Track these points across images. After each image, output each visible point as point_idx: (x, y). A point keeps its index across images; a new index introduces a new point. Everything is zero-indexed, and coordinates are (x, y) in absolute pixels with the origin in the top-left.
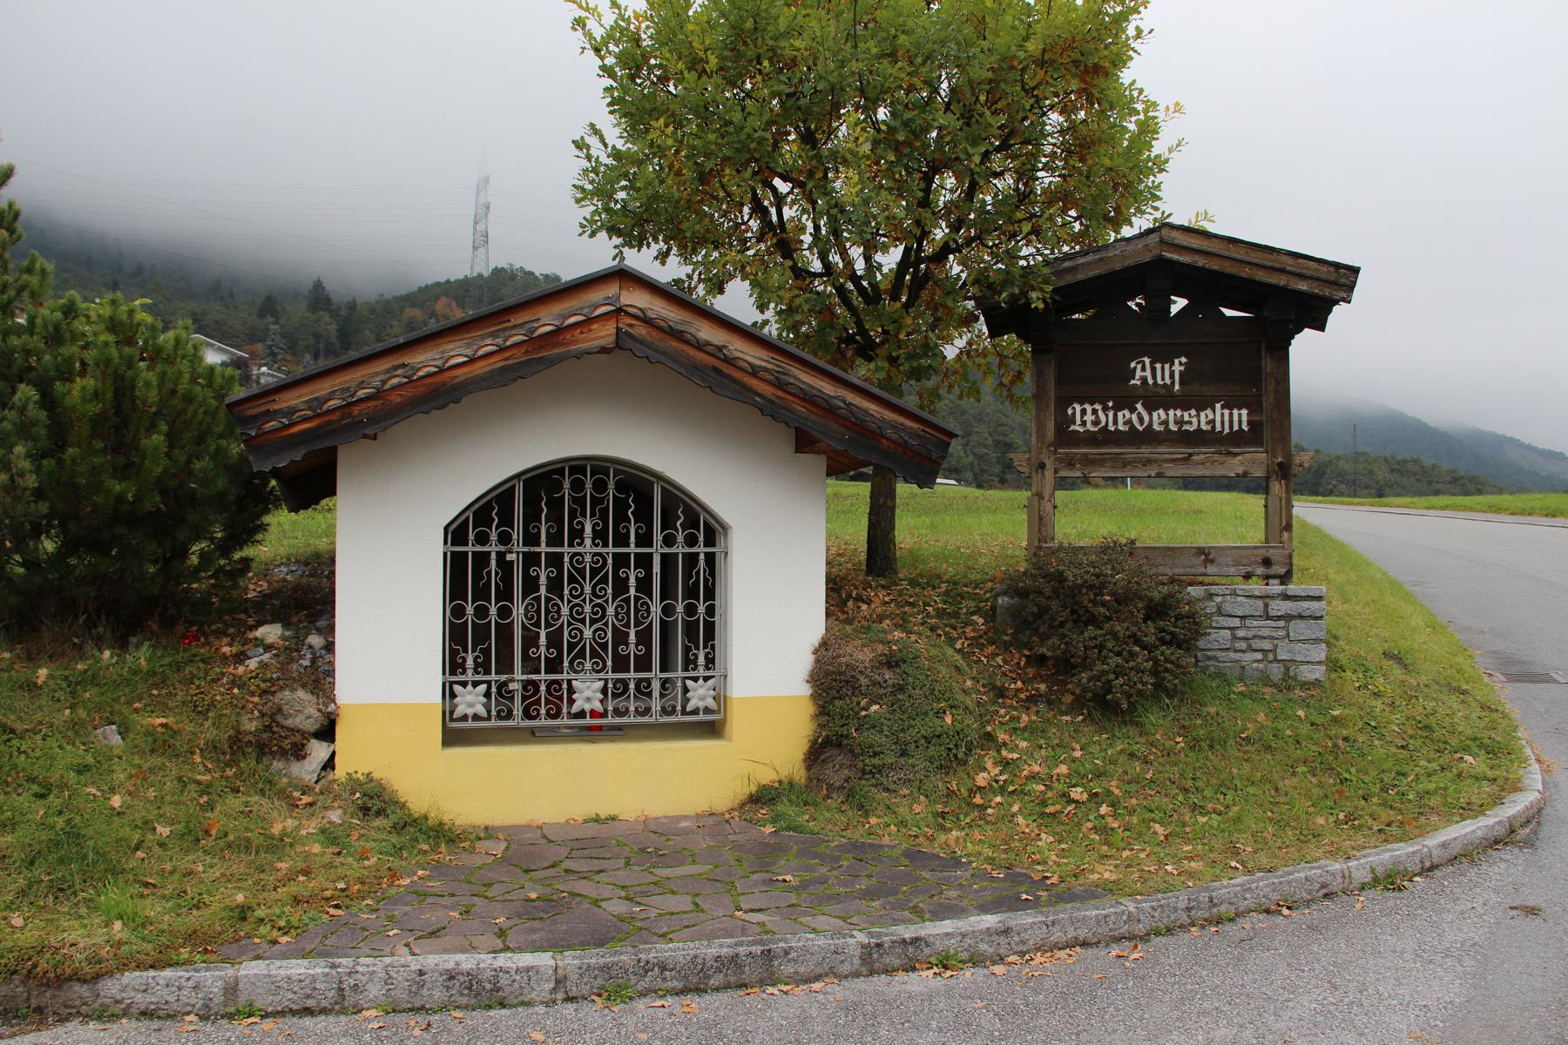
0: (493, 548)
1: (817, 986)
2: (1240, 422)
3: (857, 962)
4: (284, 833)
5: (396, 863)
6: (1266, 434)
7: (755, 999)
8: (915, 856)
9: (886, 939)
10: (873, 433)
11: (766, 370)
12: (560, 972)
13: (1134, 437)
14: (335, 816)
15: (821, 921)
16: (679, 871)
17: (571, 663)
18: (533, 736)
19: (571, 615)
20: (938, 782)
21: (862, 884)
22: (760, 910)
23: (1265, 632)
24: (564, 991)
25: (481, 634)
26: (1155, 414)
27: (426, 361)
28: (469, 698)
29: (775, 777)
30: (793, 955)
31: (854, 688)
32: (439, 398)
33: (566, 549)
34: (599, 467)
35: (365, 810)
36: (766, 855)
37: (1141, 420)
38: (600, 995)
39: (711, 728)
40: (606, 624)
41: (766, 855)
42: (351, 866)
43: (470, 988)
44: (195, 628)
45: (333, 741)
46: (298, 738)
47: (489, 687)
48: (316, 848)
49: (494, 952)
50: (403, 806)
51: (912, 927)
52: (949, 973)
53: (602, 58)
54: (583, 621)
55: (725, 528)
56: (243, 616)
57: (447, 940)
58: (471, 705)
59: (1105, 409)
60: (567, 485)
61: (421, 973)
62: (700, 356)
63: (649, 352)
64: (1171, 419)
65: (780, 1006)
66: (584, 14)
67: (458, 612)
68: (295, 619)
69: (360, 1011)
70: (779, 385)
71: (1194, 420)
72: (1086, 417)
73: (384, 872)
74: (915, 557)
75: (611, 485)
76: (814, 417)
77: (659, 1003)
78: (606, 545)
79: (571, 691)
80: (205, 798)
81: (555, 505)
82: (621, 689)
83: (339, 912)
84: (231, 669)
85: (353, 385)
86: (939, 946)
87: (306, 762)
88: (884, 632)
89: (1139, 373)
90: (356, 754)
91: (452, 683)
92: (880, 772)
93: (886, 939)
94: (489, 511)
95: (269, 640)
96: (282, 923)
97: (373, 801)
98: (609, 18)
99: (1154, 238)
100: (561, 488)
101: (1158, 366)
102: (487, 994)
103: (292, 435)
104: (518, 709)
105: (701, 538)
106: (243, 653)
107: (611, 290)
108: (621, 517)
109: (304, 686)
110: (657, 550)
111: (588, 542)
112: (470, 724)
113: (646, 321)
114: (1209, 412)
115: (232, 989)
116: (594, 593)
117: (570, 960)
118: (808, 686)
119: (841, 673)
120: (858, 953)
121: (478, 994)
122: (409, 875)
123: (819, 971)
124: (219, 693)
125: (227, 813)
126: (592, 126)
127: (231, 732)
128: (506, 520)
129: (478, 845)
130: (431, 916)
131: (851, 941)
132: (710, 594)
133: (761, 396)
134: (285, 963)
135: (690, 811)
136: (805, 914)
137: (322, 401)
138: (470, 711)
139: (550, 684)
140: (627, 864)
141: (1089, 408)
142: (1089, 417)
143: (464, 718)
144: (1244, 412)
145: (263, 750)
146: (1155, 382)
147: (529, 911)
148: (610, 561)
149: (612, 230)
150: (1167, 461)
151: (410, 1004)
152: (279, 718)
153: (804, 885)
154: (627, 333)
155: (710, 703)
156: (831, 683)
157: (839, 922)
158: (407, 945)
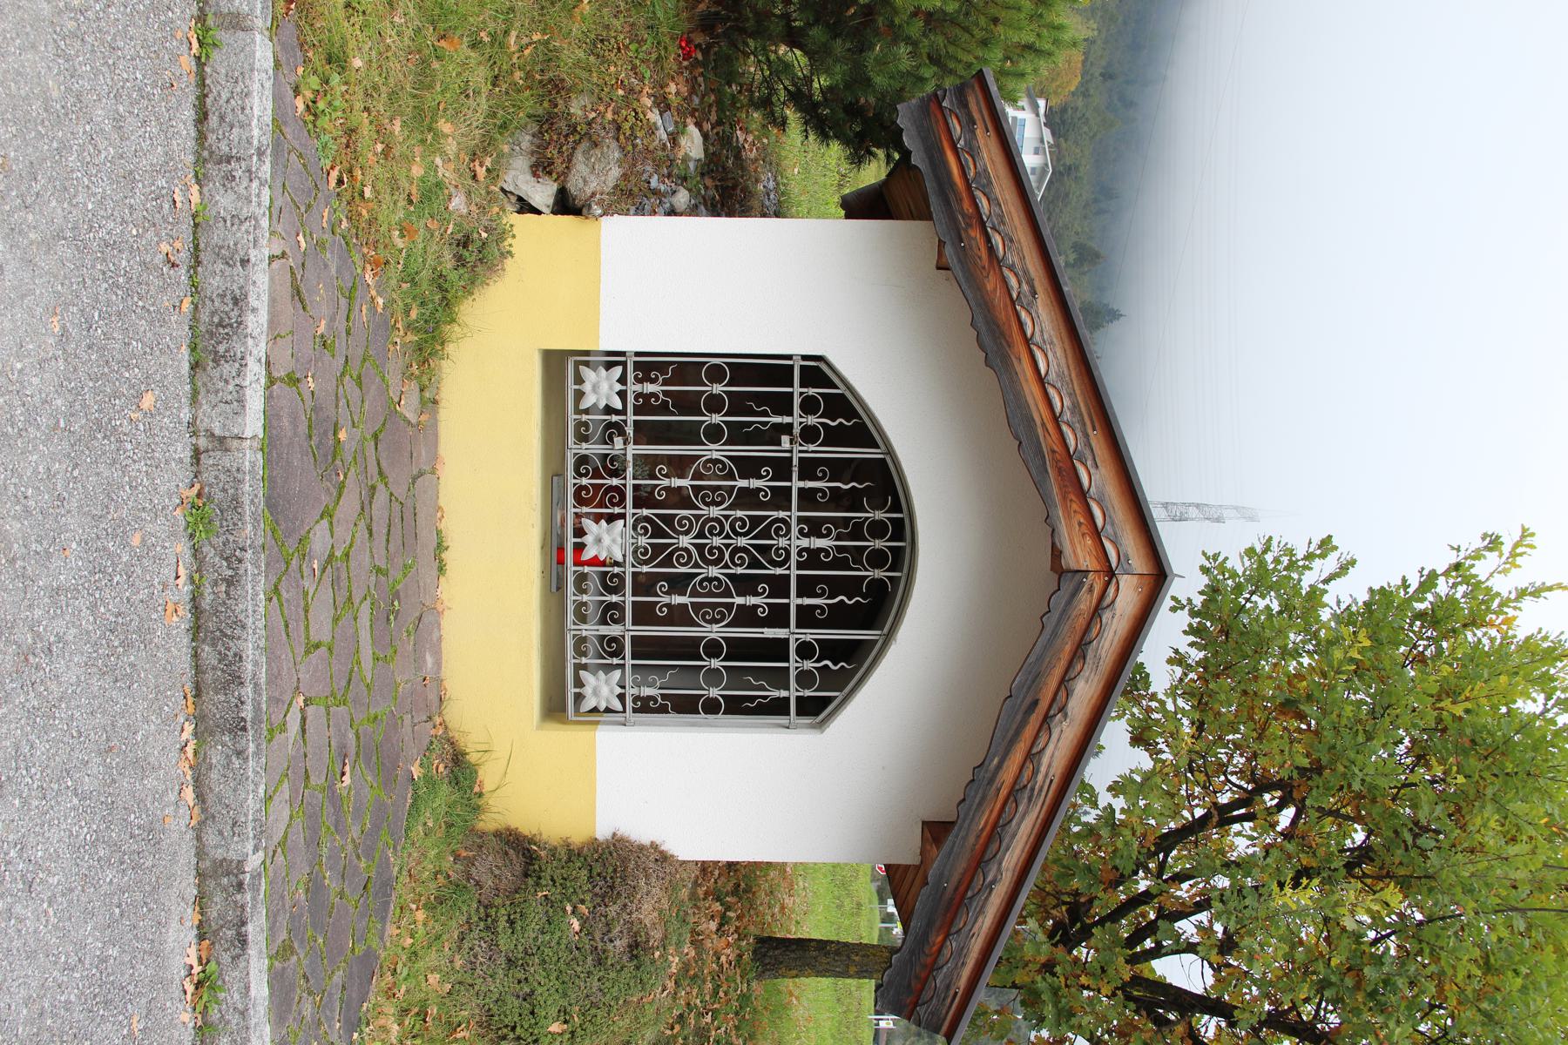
0: (797, 419)
1: (189, 794)
3: (219, 854)
4: (438, 135)
5: (395, 272)
7: (177, 703)
8: (367, 967)
9: (248, 896)
10: (951, 923)
11: (1035, 772)
12: (235, 443)
14: (458, 203)
15: (281, 812)
16: (365, 636)
17: (647, 519)
18: (552, 475)
19: (710, 520)
21: (330, 880)
22: (304, 731)
24: (208, 448)
25: (687, 404)
27: (1041, 321)
28: (604, 387)
29: (488, 787)
30: (236, 763)
31: (603, 897)
32: (995, 339)
33: (795, 513)
34: (900, 558)
35: (465, 242)
36: (381, 758)
38: (199, 495)
39: (558, 704)
40: (696, 565)
41: (381, 758)
42: (392, 213)
43: (220, 324)
44: (700, 57)
45: (554, 213)
46: (560, 168)
47: (617, 412)
48: (417, 171)
49: (268, 364)
50: (468, 291)
51: (262, 938)
52: (190, 989)
53: (1446, 574)
54: (701, 535)
55: (821, 726)
56: (713, 117)
57: (288, 309)
58: (595, 388)
60: (879, 515)
61: (245, 262)
62: (1053, 683)
63: (1055, 615)
65: (166, 739)
66: (1506, 549)
67: (716, 374)
68: (709, 182)
69: (198, 182)
73: (383, 254)
74: (780, 1010)
75: (878, 574)
76: (972, 839)
77: (182, 571)
78: (800, 566)
79: (611, 519)
80: (486, 39)
81: (851, 501)
82: (611, 584)
83: (333, 183)
84: (647, 89)
85: (1007, 229)
86: (231, 976)
87: (529, 177)
88: (679, 944)
90: (537, 240)
91: (624, 364)
92: (487, 928)
93: (248, 896)
94: (844, 416)
95: (683, 141)
96: (321, 105)
97: (476, 255)
98: (1503, 585)
100: (874, 508)
102: (211, 345)
103: (943, 153)
104: (593, 449)
105: (808, 693)
106: (668, 107)
108: (836, 586)
109: (625, 176)
110: (793, 634)
111: (805, 542)
112: (571, 387)
113: (1097, 611)
115: (237, 22)
116: (737, 550)
117: (250, 458)
118: (608, 835)
119: (624, 879)
120: (232, 855)
121: (212, 334)
122: (378, 286)
123: (210, 798)
124: (618, 69)
125: (463, 64)
126: (1353, 563)
127: (569, 82)
128: (834, 437)
129: (414, 386)
130: (321, 296)
131: (250, 847)
132: (736, 707)
134: (268, 93)
135: (445, 673)
136: (294, 790)
138: (587, 387)
139: (620, 491)
140: (379, 570)
143: (579, 380)
145: (546, 122)
147: (321, 427)
148: (779, 571)
149: (1213, 591)
151: (202, 245)
152: (585, 145)
153: (335, 799)
154: (1081, 584)
156: (611, 866)
157: (278, 836)
158: (284, 255)
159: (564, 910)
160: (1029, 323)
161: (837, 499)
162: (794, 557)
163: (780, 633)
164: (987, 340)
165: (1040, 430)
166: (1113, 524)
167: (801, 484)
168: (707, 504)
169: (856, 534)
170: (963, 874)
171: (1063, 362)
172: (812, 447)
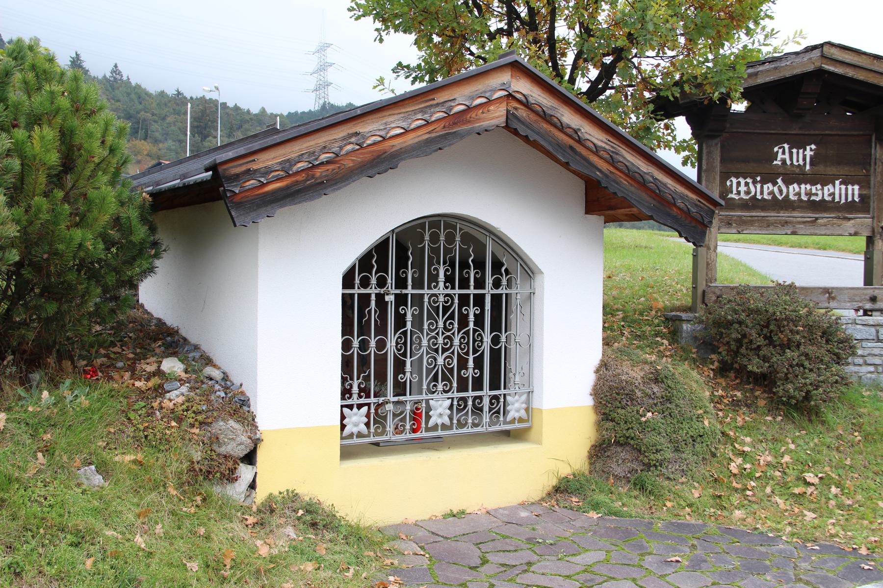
0: (373, 291)
2: (853, 195)
6: (873, 204)
10: (668, 202)
11: (605, 150)
13: (776, 204)
19: (429, 346)
20: (703, 470)
23: (876, 351)
25: (364, 362)
26: (791, 187)
37: (781, 191)
40: (453, 353)
46: (230, 464)
54: (437, 351)
59: (755, 182)
60: (427, 238)
64: (803, 191)
70: (612, 162)
71: (820, 193)
72: (741, 188)
75: (458, 238)
76: (633, 189)
85: (317, 150)
87: (237, 484)
89: (780, 156)
94: (373, 261)
99: (817, 53)
100: (423, 240)
101: (795, 151)
107: (505, 77)
110: (488, 291)
113: (527, 105)
114: (830, 186)
116: (445, 328)
118: (591, 398)
128: (383, 267)
133: (600, 171)
137: (291, 163)
141: (742, 181)
142: (743, 188)
144: (856, 187)
146: (792, 164)
148: (456, 301)
150: (799, 223)
154: (513, 114)
155: (523, 413)
159: (646, 422)
160: (374, 138)
161: (419, 265)
162: (449, 291)
163: (488, 300)
164: (382, 168)
165: (433, 135)
166: (485, 92)
167: (410, 287)
168: (421, 347)
169: (435, 251)
170: (651, 197)
171: (396, 117)
172: (389, 281)
